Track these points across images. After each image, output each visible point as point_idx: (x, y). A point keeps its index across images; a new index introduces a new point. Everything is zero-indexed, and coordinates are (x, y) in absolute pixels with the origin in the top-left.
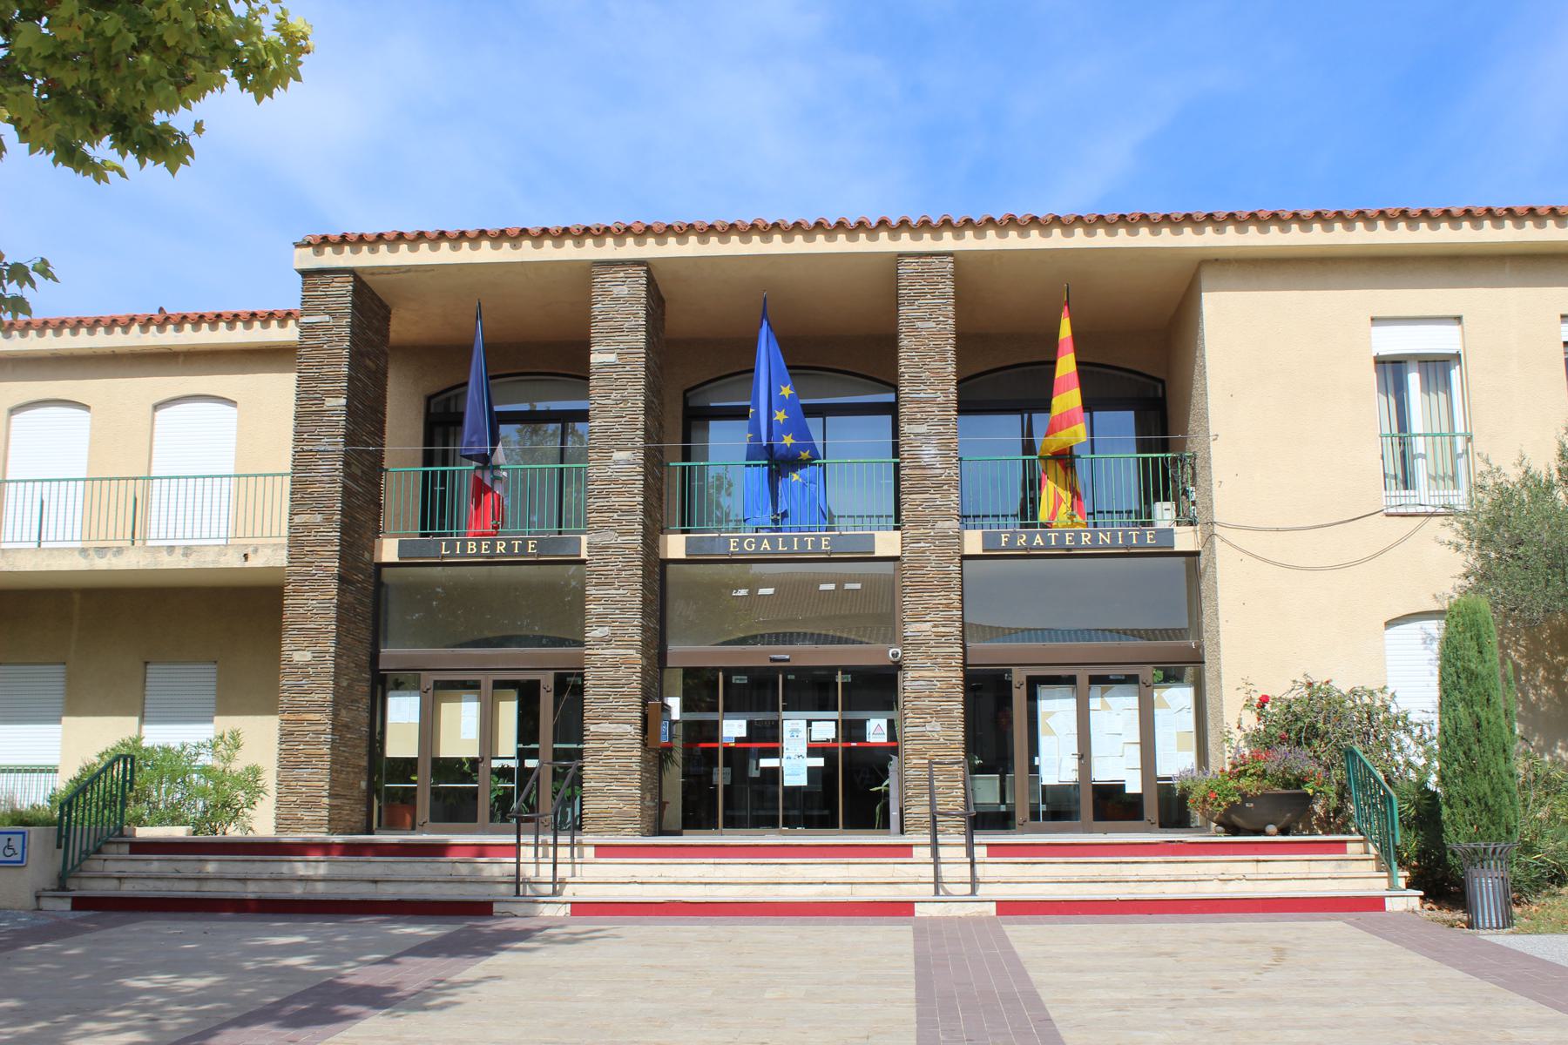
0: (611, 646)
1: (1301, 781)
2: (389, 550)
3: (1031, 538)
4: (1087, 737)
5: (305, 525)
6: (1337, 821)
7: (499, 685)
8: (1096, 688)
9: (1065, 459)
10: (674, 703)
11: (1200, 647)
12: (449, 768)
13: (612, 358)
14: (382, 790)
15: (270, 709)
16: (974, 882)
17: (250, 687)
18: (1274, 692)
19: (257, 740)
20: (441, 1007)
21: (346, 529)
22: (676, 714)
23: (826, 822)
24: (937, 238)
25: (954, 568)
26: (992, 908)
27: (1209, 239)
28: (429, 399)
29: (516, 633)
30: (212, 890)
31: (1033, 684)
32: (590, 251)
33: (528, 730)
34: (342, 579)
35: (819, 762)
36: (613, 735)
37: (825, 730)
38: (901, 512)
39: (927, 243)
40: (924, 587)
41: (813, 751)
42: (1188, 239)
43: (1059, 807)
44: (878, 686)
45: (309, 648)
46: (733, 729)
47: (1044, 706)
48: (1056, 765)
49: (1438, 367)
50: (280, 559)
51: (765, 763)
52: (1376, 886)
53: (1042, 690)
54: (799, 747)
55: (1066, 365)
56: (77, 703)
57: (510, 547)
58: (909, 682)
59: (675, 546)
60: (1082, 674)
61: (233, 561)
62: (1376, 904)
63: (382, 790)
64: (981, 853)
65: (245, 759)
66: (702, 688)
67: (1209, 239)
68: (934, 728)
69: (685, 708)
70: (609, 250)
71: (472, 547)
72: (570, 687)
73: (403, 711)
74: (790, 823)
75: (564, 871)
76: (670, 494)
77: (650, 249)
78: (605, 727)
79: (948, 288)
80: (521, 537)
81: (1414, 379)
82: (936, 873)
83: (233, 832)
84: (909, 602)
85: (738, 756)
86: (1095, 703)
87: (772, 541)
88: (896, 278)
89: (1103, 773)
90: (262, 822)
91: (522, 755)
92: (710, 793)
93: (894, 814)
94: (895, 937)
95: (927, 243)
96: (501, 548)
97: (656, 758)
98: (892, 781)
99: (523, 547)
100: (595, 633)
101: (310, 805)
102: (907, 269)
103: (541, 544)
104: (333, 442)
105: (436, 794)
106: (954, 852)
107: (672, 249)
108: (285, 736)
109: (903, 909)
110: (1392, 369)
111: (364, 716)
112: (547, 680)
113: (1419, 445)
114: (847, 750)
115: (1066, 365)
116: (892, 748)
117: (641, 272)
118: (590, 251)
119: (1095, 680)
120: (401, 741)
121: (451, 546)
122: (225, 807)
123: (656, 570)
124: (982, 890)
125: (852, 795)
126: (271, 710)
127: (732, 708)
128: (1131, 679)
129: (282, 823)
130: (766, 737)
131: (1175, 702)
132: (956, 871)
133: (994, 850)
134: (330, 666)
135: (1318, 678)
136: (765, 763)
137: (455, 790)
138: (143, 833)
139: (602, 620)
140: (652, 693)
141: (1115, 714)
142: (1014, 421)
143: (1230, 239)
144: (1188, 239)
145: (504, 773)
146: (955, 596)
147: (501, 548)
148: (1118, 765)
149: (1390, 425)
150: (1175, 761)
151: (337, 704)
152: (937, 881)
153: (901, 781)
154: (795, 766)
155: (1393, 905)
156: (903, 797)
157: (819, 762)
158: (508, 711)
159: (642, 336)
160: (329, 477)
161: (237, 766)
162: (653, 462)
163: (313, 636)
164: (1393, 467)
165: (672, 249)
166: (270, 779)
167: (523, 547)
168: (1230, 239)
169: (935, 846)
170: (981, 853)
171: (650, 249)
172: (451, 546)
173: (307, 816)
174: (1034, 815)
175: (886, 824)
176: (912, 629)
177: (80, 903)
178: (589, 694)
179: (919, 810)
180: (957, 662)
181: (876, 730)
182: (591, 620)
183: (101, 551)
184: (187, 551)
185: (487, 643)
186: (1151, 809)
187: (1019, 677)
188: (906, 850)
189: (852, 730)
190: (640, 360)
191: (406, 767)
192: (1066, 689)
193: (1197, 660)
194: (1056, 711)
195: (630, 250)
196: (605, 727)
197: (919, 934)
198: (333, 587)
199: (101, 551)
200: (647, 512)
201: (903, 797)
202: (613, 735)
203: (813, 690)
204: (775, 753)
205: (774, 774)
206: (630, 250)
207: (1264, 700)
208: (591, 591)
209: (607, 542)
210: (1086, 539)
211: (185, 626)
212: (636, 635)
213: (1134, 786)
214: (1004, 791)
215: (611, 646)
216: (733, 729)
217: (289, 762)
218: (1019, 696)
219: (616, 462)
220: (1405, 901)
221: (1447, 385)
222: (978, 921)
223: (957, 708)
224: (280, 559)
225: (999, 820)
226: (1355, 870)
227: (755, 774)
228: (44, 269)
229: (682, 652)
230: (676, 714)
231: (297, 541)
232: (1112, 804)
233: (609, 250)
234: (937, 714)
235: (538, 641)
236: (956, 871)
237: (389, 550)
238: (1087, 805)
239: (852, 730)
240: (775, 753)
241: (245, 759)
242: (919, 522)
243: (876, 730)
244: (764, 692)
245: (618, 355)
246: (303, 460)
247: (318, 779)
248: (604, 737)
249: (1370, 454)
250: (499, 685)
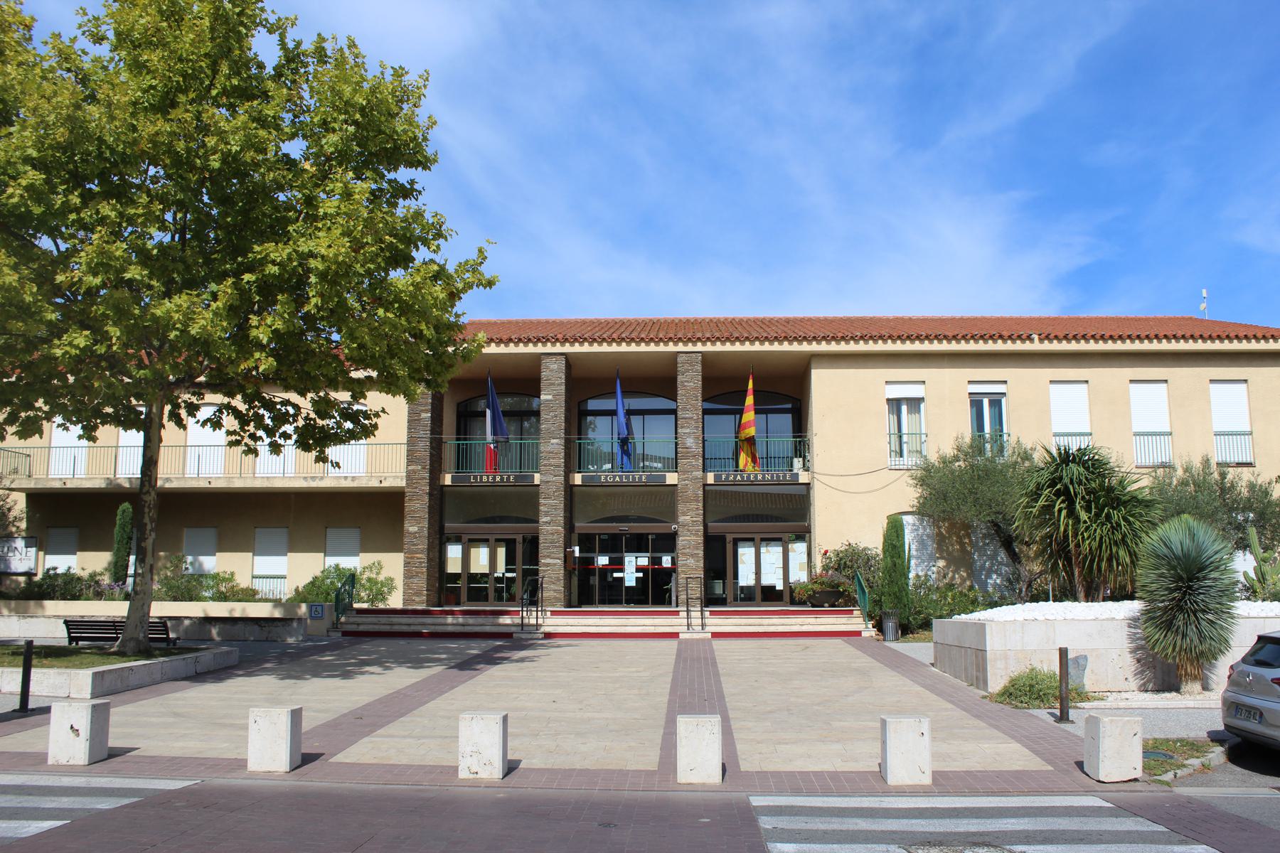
0: (551, 523)
1: (838, 585)
2: (448, 480)
3: (735, 476)
4: (761, 564)
5: (414, 471)
6: (851, 601)
7: (498, 540)
8: (764, 543)
9: (751, 441)
10: (577, 549)
11: (810, 525)
12: (474, 578)
13: (550, 397)
14: (445, 588)
15: (397, 549)
16: (703, 626)
17: (393, 542)
18: (830, 548)
19: (392, 565)
20: (522, 660)
21: (432, 472)
22: (577, 554)
23: (644, 602)
24: (695, 345)
25: (701, 492)
26: (709, 635)
27: (814, 347)
28: (458, 405)
29: (505, 516)
30: (397, 628)
31: (736, 542)
32: (540, 349)
33: (510, 560)
34: (431, 494)
35: (641, 575)
36: (552, 566)
37: (644, 561)
38: (678, 454)
39: (690, 348)
40: (688, 501)
41: (638, 569)
42: (805, 347)
43: (748, 596)
44: (668, 542)
45: (416, 526)
46: (603, 560)
47: (741, 551)
48: (746, 577)
49: (915, 403)
50: (403, 484)
51: (616, 575)
52: (861, 627)
53: (740, 544)
54: (631, 569)
55: (750, 400)
56: (294, 546)
57: (502, 479)
58: (681, 541)
59: (578, 479)
60: (757, 537)
61: (374, 483)
62: (858, 634)
63: (445, 588)
64: (707, 614)
65: (390, 575)
66: (587, 542)
67: (814, 347)
68: (691, 561)
69: (581, 551)
70: (549, 348)
71: (485, 478)
72: (532, 544)
73: (454, 552)
74: (628, 602)
75: (540, 621)
76: (575, 457)
77: (567, 348)
78: (548, 561)
79: (699, 367)
80: (504, 476)
81: (904, 408)
82: (690, 623)
83: (381, 606)
84: (681, 507)
85: (604, 571)
86: (763, 550)
87: (621, 477)
88: (676, 363)
89: (766, 581)
90: (395, 601)
91: (508, 571)
92: (591, 589)
93: (674, 598)
94: (673, 643)
95: (690, 348)
96: (498, 479)
97: (569, 574)
98: (673, 584)
99: (508, 478)
100: (543, 519)
101: (418, 594)
102: (680, 359)
103: (516, 478)
104: (425, 433)
105: (470, 589)
106: (696, 614)
107: (577, 348)
108: (407, 564)
109: (674, 635)
110: (894, 405)
111: (437, 554)
112: (519, 538)
113: (905, 438)
114: (653, 570)
115: (750, 400)
116: (673, 570)
117: (563, 358)
118: (540, 349)
119: (762, 540)
120: (454, 567)
121: (475, 477)
122: (381, 596)
123: (570, 489)
124: (707, 629)
125: (655, 590)
126: (401, 551)
127: (603, 551)
128: (779, 540)
129: (405, 601)
130: (618, 564)
131: (799, 549)
132: (696, 621)
133: (712, 613)
134: (426, 533)
135: (853, 542)
136: (616, 575)
137: (477, 588)
138: (356, 606)
139: (547, 514)
140: (568, 544)
141: (772, 555)
142: (730, 419)
143: (824, 347)
144: (805, 347)
145: (499, 580)
146: (701, 505)
147: (498, 479)
148: (773, 577)
149: (894, 430)
150: (799, 575)
151: (428, 549)
152: (689, 625)
153: (677, 584)
154: (630, 577)
155: (864, 634)
156: (677, 591)
157: (641, 575)
158: (501, 552)
159: (563, 387)
160: (424, 447)
161: (381, 578)
162: (568, 443)
163: (418, 520)
164: (895, 446)
165: (577, 348)
166: (399, 582)
167: (508, 478)
168: (824, 347)
169: (688, 611)
170: (707, 614)
171: (567, 348)
172: (475, 477)
173: (417, 599)
174: (735, 599)
175: (670, 603)
176: (681, 519)
177: (345, 634)
178: (541, 546)
179: (683, 597)
180: (701, 533)
181: (666, 561)
182: (542, 514)
183: (313, 478)
184: (354, 478)
185: (487, 520)
186: (787, 597)
187: (729, 538)
188: (677, 613)
189: (656, 561)
190: (563, 398)
191: (456, 577)
192: (751, 543)
193: (808, 530)
194: (746, 554)
195: (558, 348)
196: (548, 561)
197: (680, 643)
198: (427, 498)
199: (313, 478)
200: (566, 466)
201: (677, 591)
202: (552, 566)
203: (638, 544)
204: (622, 570)
205: (621, 580)
206: (558, 348)
207: (826, 552)
208: (542, 501)
209: (547, 478)
210: (760, 477)
211: (370, 514)
212: (561, 519)
213: (780, 587)
214: (719, 587)
215: (551, 523)
216: (603, 560)
217: (408, 575)
218: (729, 547)
219: (552, 445)
220: (869, 631)
221: (919, 412)
222: (703, 640)
223: (701, 553)
224: (403, 484)
225: (721, 601)
226: (855, 621)
227: (610, 579)
228: (383, 411)
229: (581, 526)
230: (577, 554)
231: (410, 476)
232: (770, 594)
233: (549, 348)
234: (692, 556)
235: (518, 520)
236: (696, 621)
237: (448, 480)
238: (758, 595)
239: (656, 561)
240: (622, 570)
241: (390, 575)
242: (685, 472)
243: (666, 561)
244: (615, 546)
245: (552, 396)
246: (411, 442)
247: (421, 583)
248: (548, 565)
249: (882, 443)
250: (498, 540)
